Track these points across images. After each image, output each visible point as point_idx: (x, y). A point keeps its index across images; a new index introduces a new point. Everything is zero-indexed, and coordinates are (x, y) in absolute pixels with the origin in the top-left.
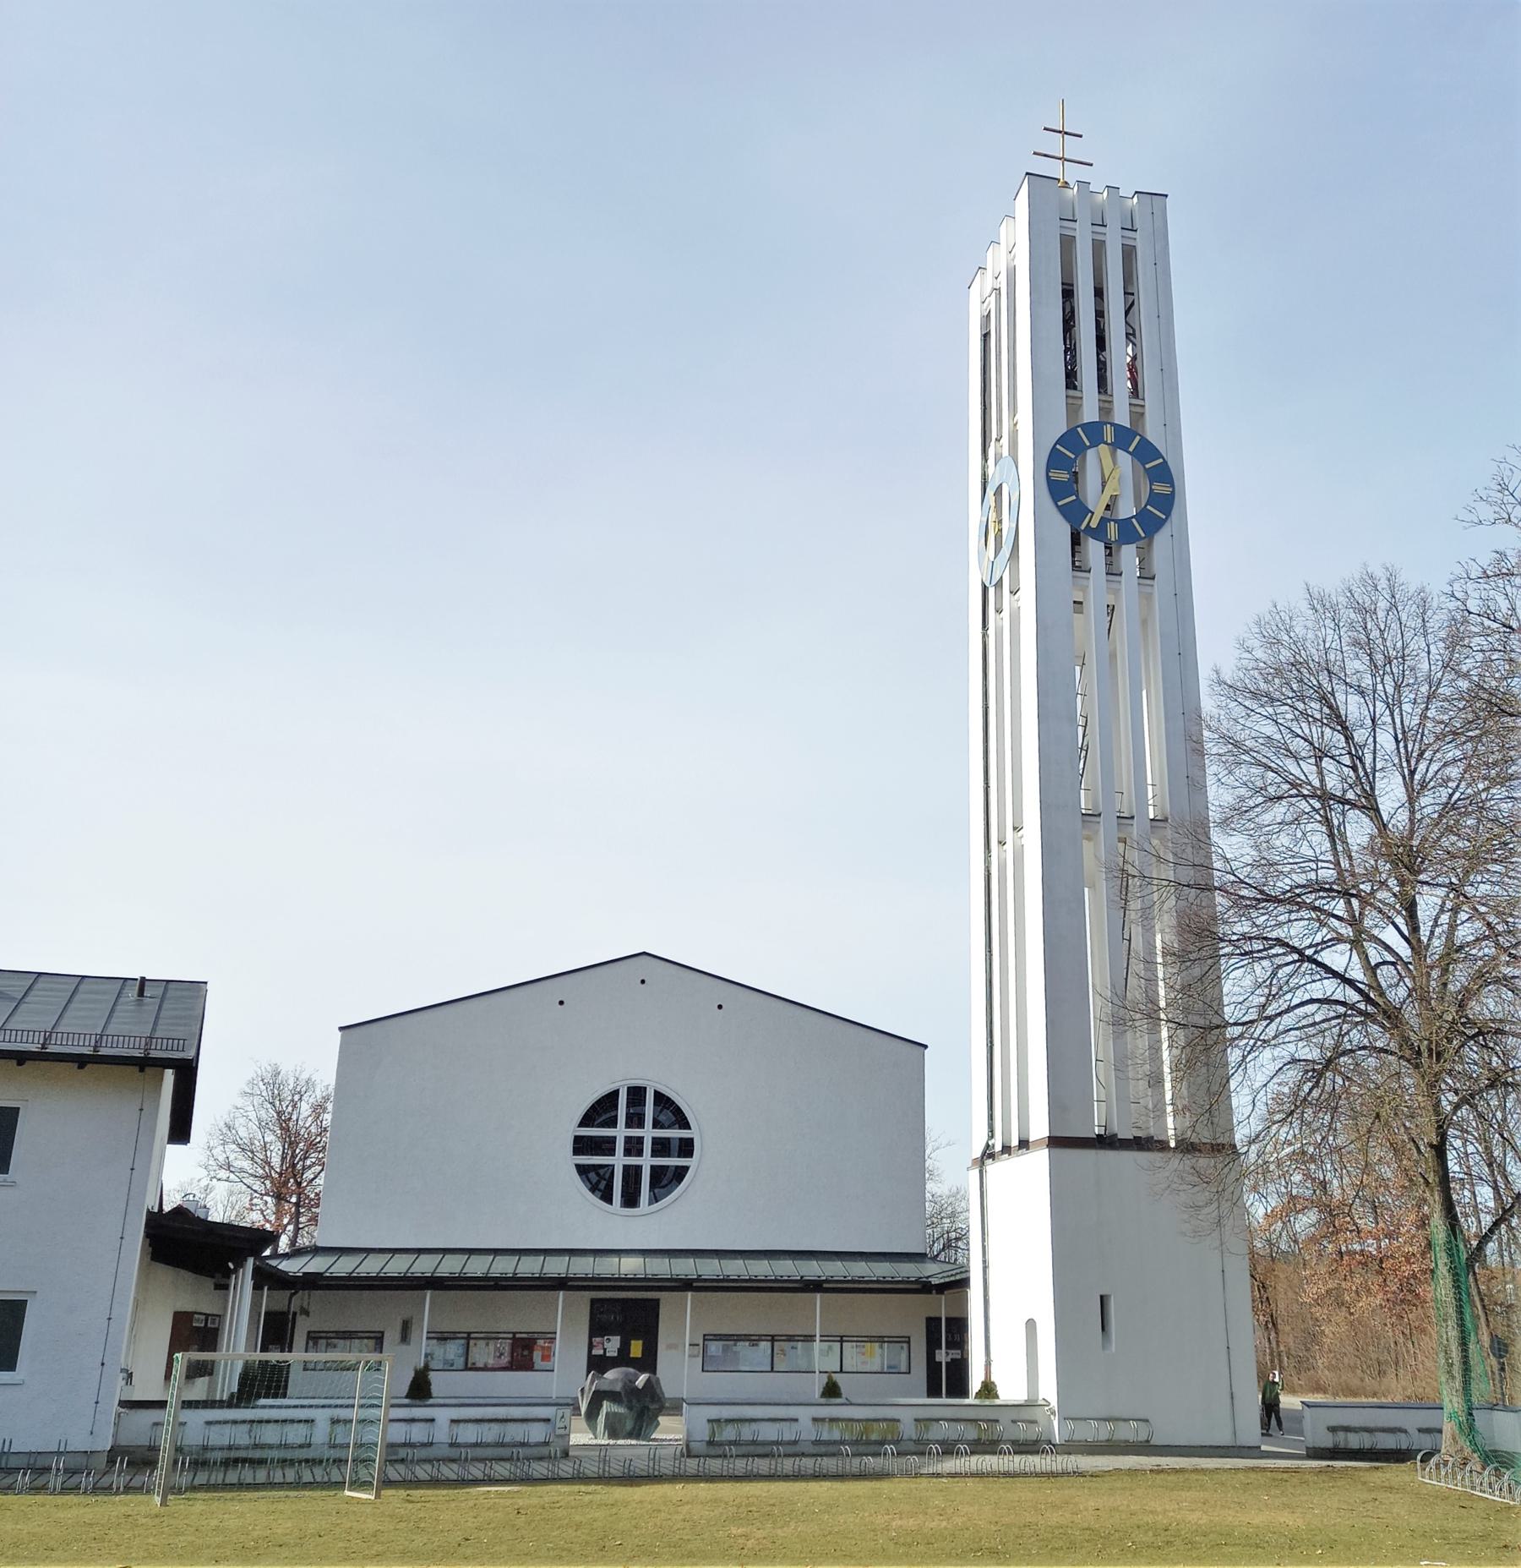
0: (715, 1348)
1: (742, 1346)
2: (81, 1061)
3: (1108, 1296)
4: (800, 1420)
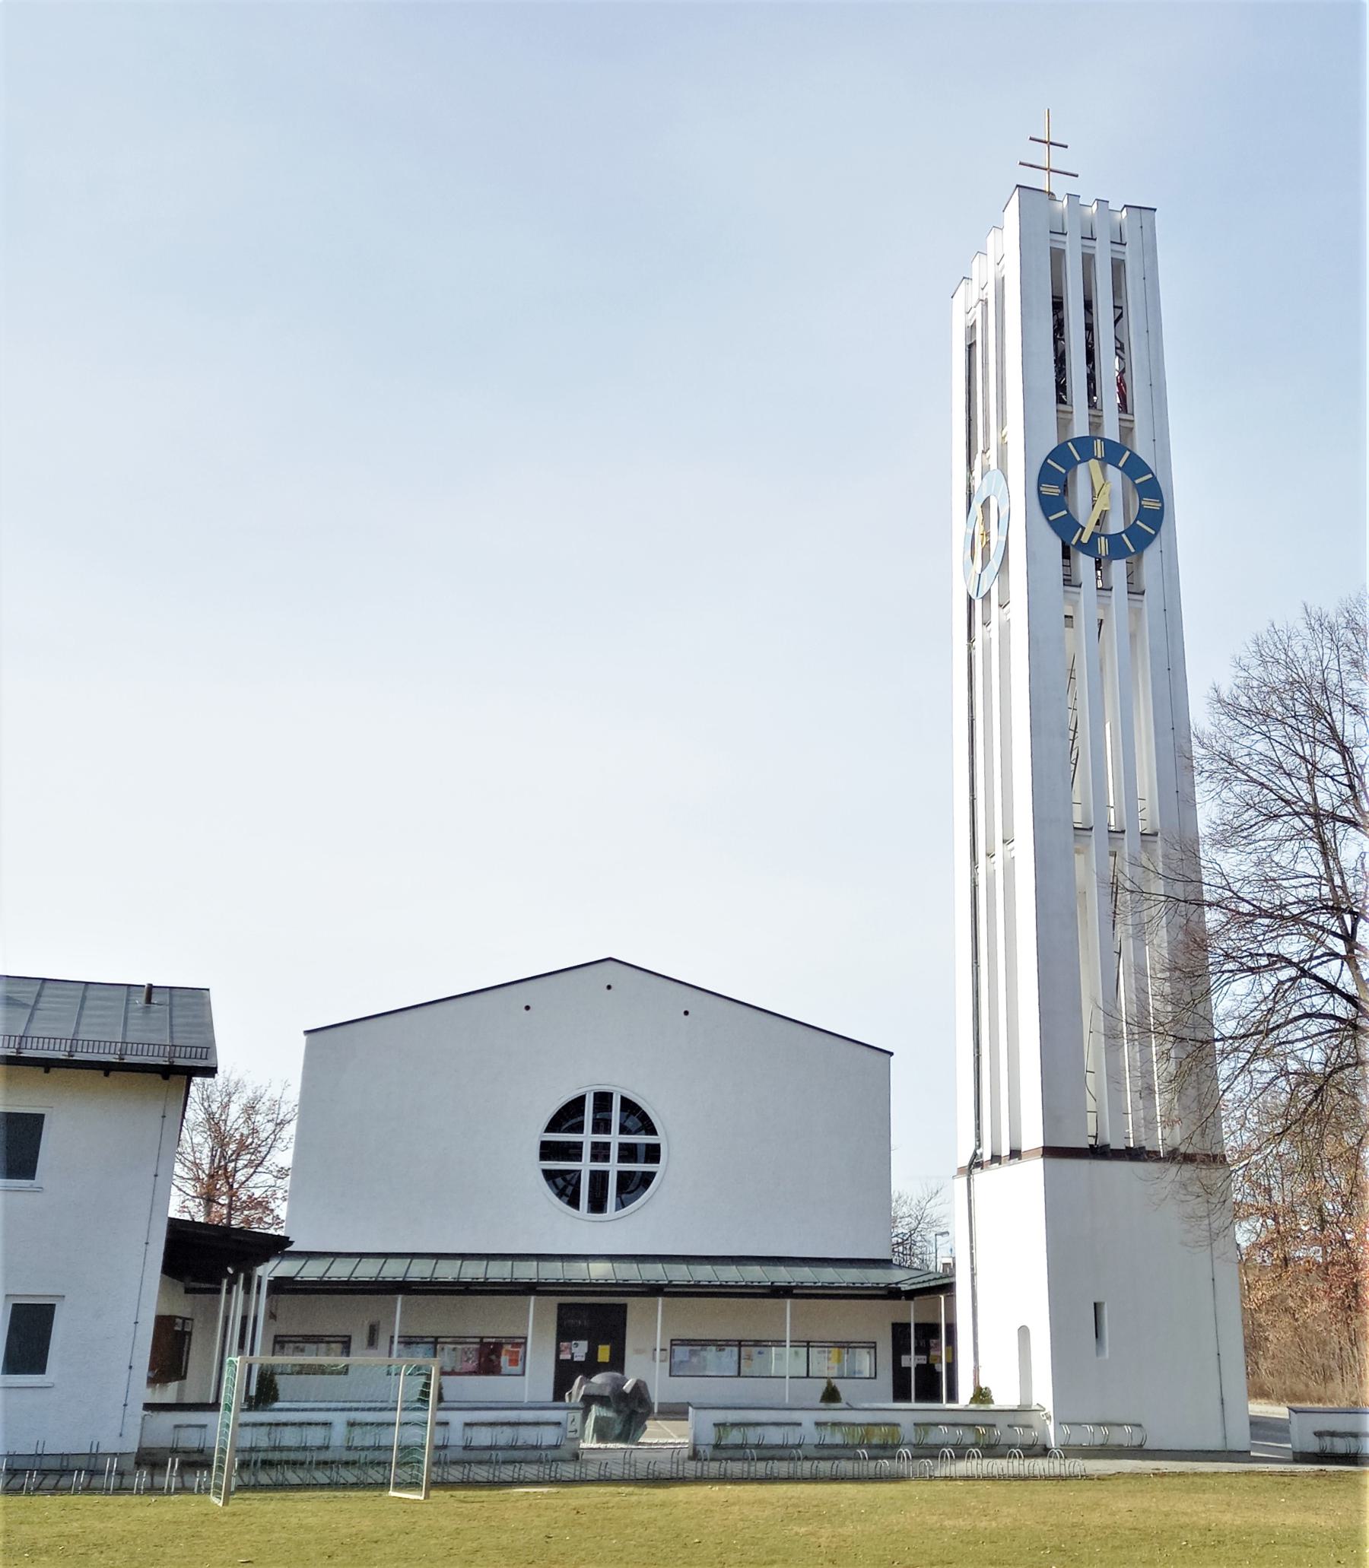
0: (681, 1352)
1: (711, 1353)
2: (107, 1068)
4: (803, 1425)
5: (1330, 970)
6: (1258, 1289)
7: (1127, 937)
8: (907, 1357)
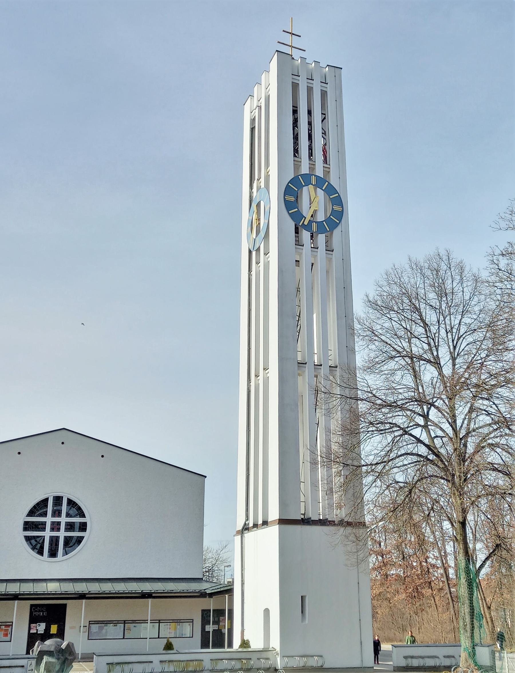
0: (95, 628)
3: (305, 596)
5: (417, 432)
6: (374, 589)
7: (322, 416)
8: (209, 626)
